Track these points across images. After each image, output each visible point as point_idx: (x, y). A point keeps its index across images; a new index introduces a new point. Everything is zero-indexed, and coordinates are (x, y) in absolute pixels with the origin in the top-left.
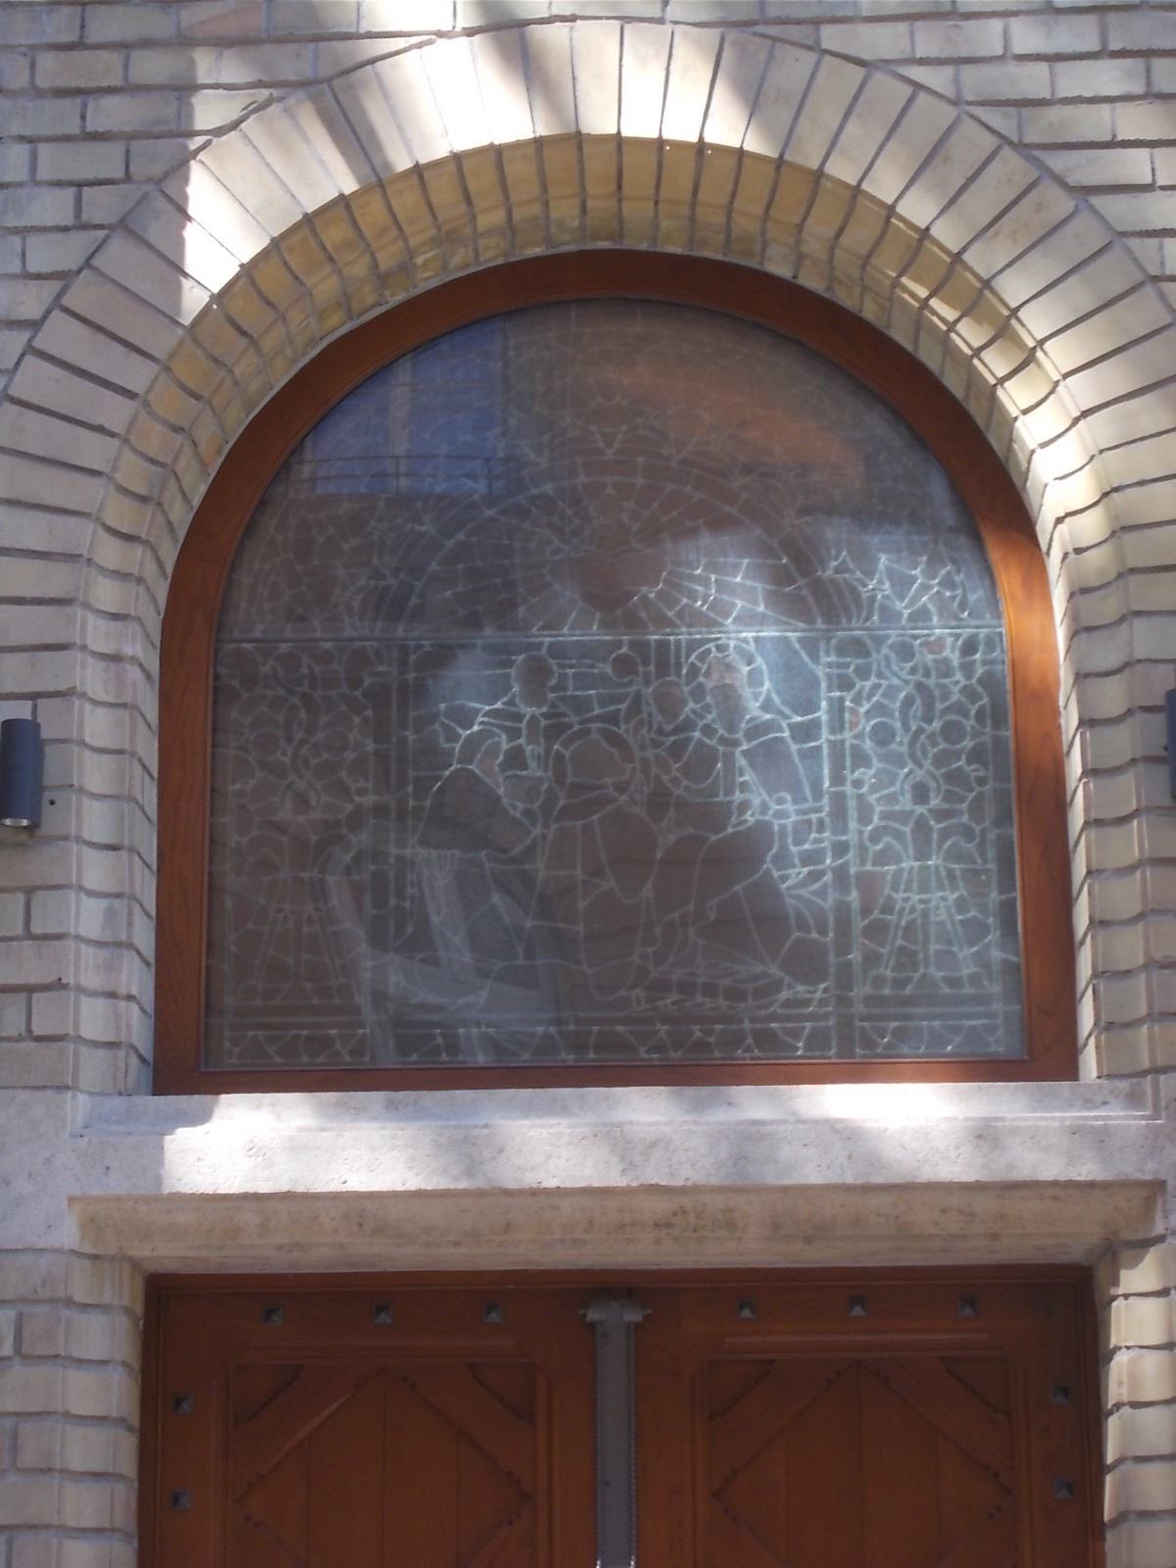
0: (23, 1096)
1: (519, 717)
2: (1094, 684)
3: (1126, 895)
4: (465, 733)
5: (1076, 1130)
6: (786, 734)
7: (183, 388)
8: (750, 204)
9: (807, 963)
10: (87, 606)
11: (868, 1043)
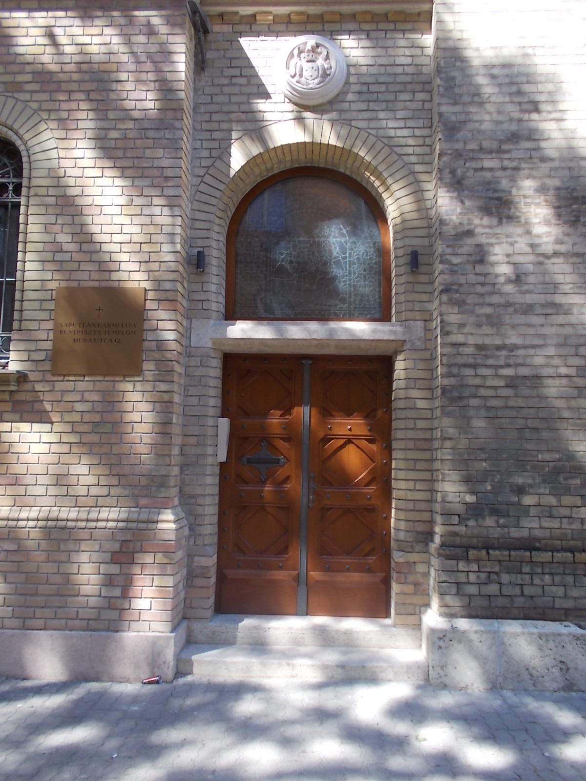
0: (202, 320)
1: (292, 254)
2: (398, 250)
3: (402, 289)
4: (282, 257)
5: (391, 331)
6: (341, 259)
7: (231, 190)
8: (337, 157)
9: (343, 301)
10: (213, 230)
11: (353, 315)
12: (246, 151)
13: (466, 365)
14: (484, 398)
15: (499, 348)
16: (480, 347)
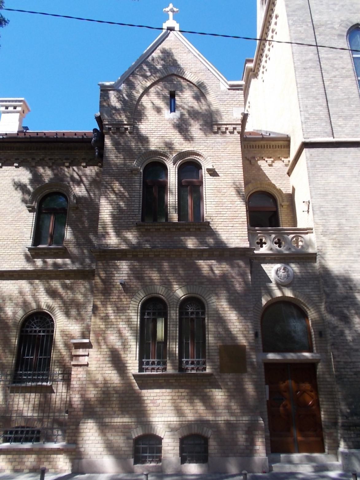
12: (266, 300)
13: (341, 368)
14: (348, 378)
15: (351, 362)
16: (345, 362)
